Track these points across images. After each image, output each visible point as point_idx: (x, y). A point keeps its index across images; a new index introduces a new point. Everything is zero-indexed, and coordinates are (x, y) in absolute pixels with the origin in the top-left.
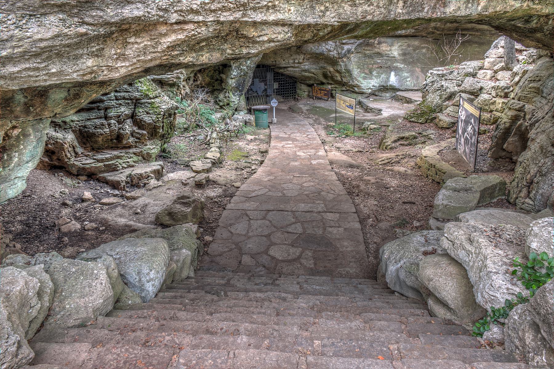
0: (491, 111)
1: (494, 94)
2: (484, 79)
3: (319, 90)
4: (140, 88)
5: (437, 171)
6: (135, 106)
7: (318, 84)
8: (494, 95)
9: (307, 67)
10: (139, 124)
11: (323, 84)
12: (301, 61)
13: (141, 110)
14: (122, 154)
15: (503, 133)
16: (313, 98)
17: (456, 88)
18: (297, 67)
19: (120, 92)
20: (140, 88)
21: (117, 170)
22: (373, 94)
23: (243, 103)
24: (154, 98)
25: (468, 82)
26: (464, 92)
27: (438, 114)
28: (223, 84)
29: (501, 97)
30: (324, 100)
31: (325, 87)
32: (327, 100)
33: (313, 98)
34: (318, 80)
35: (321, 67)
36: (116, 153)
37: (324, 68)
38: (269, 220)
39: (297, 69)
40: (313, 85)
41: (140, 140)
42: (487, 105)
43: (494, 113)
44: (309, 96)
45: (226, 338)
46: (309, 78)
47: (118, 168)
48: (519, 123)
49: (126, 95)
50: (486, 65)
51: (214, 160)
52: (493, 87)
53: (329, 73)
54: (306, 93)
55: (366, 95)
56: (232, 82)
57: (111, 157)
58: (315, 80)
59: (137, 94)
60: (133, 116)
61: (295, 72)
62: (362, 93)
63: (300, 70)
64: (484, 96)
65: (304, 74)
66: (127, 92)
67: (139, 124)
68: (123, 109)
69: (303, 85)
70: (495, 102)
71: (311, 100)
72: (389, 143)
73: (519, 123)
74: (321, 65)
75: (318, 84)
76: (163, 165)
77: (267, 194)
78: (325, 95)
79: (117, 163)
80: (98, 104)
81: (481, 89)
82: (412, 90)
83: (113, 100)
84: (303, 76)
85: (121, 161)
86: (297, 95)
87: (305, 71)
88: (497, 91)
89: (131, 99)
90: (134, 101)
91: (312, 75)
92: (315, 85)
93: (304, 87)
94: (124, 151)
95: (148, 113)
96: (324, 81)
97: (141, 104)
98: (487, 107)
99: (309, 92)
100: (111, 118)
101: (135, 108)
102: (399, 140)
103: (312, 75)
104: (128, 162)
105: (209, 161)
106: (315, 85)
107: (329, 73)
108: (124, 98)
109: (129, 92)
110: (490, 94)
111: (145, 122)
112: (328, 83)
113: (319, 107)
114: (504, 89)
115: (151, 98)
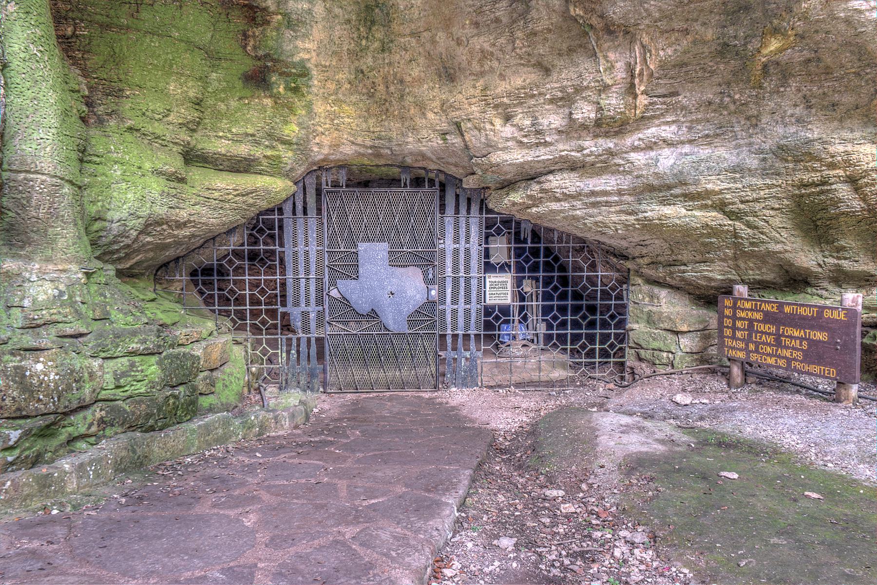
3: (768, 318)
7: (758, 286)
9: (667, 160)
11: (796, 280)
12: (613, 102)
16: (727, 376)
18: (603, 165)
30: (811, 392)
31: (808, 301)
32: (834, 397)
33: (727, 376)
34: (763, 258)
35: (782, 151)
37: (799, 155)
39: (606, 183)
44: (701, 358)
46: (701, 242)
53: (843, 191)
54: (687, 343)
58: (741, 253)
61: (595, 199)
63: (626, 182)
65: (654, 211)
69: (663, 293)
71: (719, 384)
74: (780, 133)
75: (758, 286)
78: (815, 354)
84: (648, 226)
86: (630, 354)
87: (660, 189)
91: (713, 217)
92: (742, 290)
93: (670, 306)
96: (807, 258)
99: (705, 334)
103: (713, 217)
106: (742, 290)
107: (843, 191)
112: (842, 279)
113: (753, 449)
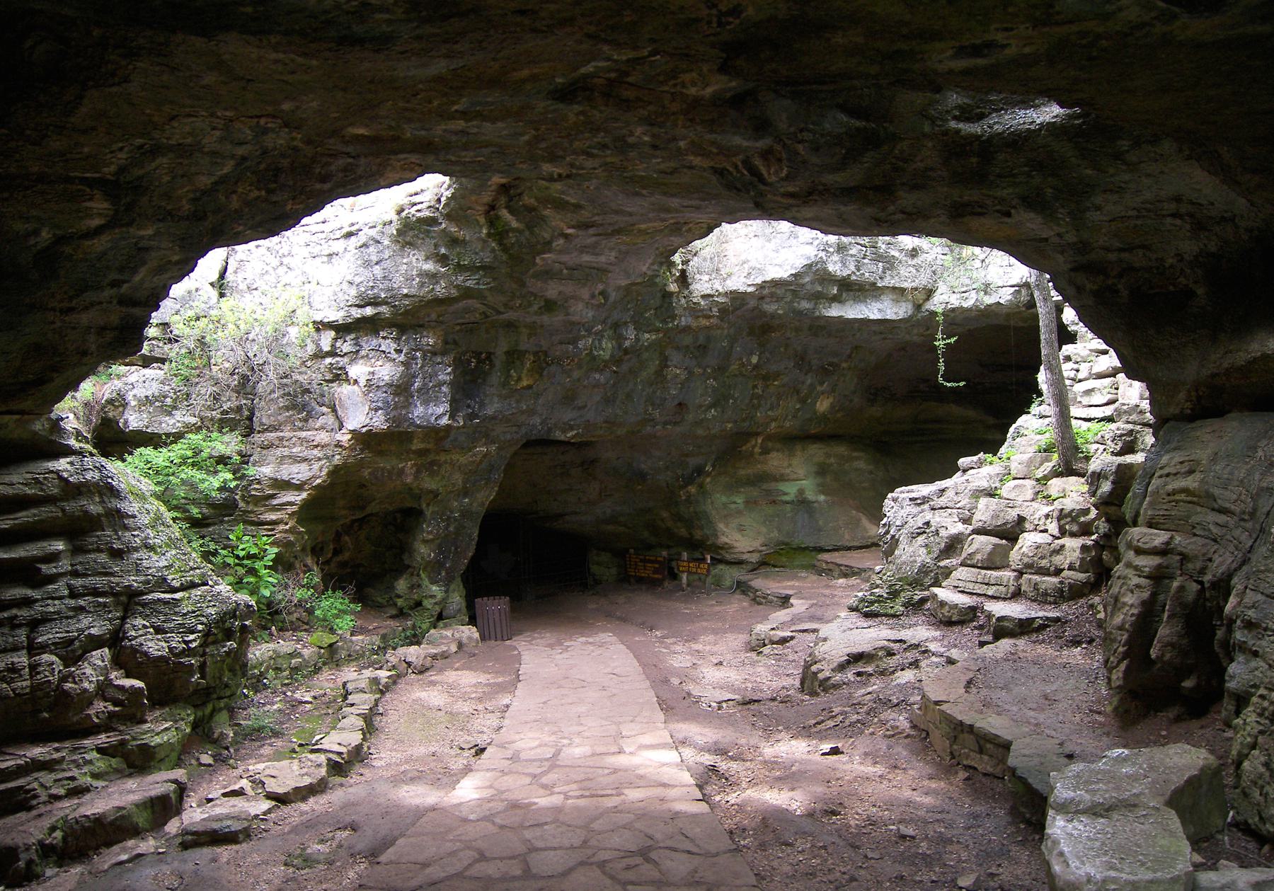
0: (1058, 572)
1: (1053, 527)
2: (1020, 498)
4: (145, 563)
5: (982, 742)
6: (126, 610)
8: (1056, 532)
10: (127, 659)
13: (139, 622)
14: (56, 756)
15: (1139, 615)
17: (960, 528)
19: (85, 575)
20: (145, 563)
21: (30, 809)
22: (763, 564)
23: (457, 600)
24: (183, 588)
25: (985, 511)
26: (978, 532)
27: (936, 590)
28: (405, 557)
29: (1073, 535)
36: (37, 752)
38: (1139, 247)
40: (627, 550)
41: (130, 710)
42: (1042, 558)
43: (1065, 573)
45: (1027, 50)
47: (34, 802)
48: (1175, 584)
49: (99, 582)
50: (1015, 468)
51: (340, 754)
52: (1047, 516)
55: (750, 567)
56: (423, 551)
57: (19, 766)
59: (133, 581)
60: (115, 640)
62: (740, 563)
64: (1028, 540)
66: (106, 574)
67: (127, 659)
68: (85, 621)
70: (1063, 546)
72: (827, 674)
73: (1175, 584)
76: (184, 779)
77: (473, 872)
78: (656, 571)
79: (35, 785)
80: (14, 611)
81: (1021, 520)
82: (849, 549)
83: (61, 598)
85: (47, 778)
88: (1062, 522)
89: (115, 595)
90: (123, 599)
92: (632, 551)
94: (67, 744)
95: (158, 630)
97: (144, 605)
98: (1044, 563)
100: (44, 648)
101: (123, 619)
102: (848, 662)
104: (73, 779)
105: (322, 758)
108: (95, 592)
109: (112, 574)
110: (1045, 531)
111: (146, 654)
114: (1078, 516)
115: (175, 590)
